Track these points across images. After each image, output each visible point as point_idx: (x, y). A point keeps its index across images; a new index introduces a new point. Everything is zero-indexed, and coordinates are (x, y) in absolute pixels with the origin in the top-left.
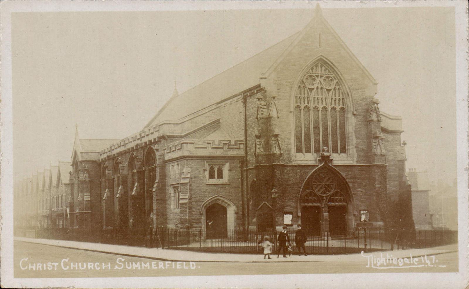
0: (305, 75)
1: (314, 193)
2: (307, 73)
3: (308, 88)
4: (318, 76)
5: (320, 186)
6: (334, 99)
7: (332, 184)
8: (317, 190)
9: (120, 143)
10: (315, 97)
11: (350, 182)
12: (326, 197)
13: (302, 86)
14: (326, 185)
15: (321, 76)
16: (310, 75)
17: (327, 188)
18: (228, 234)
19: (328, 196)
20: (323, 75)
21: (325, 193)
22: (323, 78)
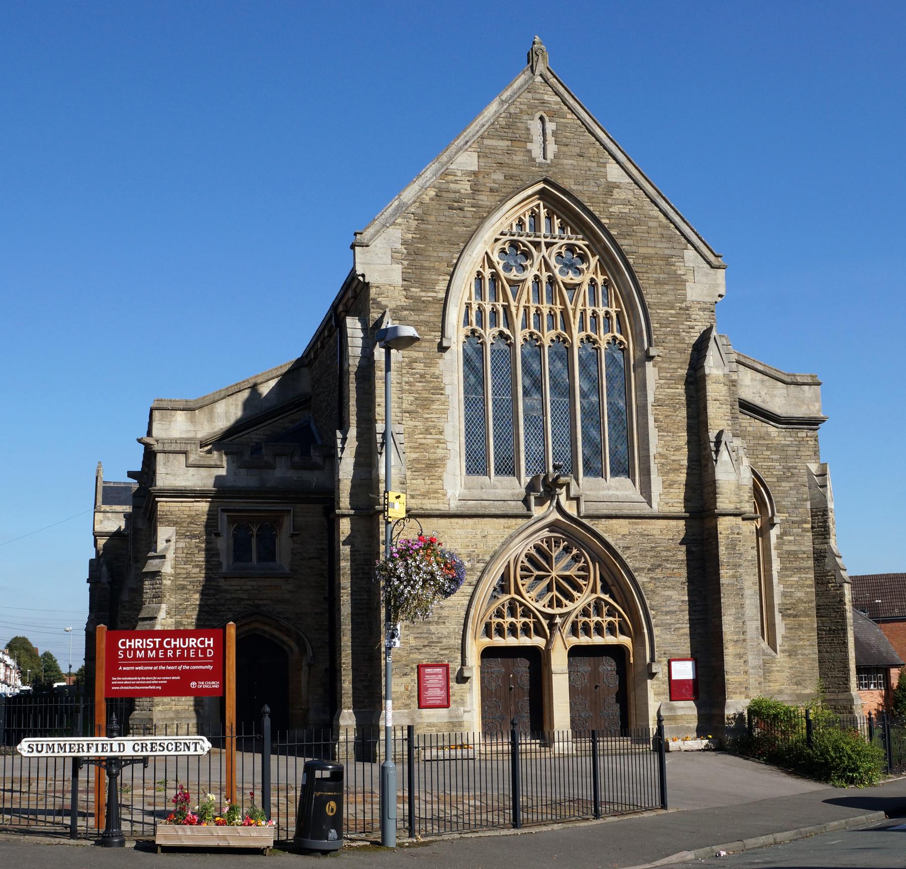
0: (497, 240)
1: (521, 604)
2: (502, 234)
3: (564, 283)
4: (539, 243)
5: (546, 582)
6: (533, 311)
7: (585, 578)
8: (533, 594)
9: (807, 711)
10: (528, 307)
11: (636, 570)
12: (561, 615)
13: (487, 273)
14: (567, 579)
15: (549, 245)
16: (511, 241)
17: (567, 588)
18: (144, 699)
19: (569, 613)
20: (554, 241)
21: (560, 604)
22: (555, 249)
